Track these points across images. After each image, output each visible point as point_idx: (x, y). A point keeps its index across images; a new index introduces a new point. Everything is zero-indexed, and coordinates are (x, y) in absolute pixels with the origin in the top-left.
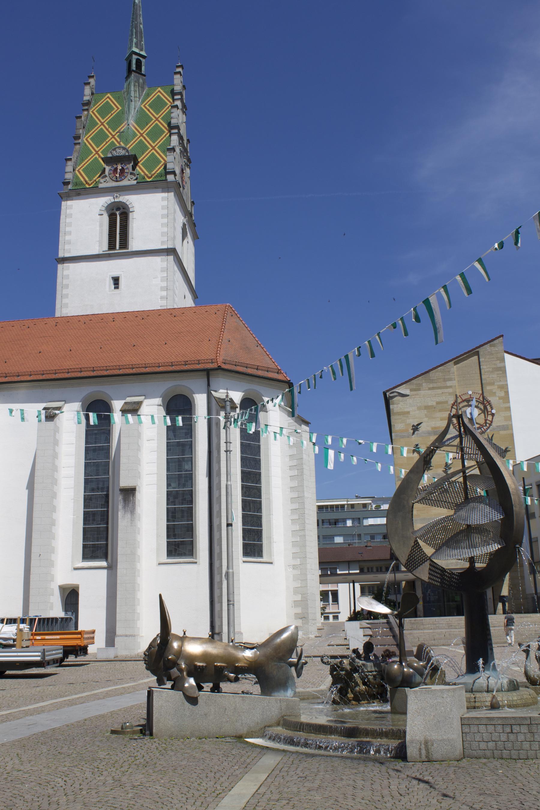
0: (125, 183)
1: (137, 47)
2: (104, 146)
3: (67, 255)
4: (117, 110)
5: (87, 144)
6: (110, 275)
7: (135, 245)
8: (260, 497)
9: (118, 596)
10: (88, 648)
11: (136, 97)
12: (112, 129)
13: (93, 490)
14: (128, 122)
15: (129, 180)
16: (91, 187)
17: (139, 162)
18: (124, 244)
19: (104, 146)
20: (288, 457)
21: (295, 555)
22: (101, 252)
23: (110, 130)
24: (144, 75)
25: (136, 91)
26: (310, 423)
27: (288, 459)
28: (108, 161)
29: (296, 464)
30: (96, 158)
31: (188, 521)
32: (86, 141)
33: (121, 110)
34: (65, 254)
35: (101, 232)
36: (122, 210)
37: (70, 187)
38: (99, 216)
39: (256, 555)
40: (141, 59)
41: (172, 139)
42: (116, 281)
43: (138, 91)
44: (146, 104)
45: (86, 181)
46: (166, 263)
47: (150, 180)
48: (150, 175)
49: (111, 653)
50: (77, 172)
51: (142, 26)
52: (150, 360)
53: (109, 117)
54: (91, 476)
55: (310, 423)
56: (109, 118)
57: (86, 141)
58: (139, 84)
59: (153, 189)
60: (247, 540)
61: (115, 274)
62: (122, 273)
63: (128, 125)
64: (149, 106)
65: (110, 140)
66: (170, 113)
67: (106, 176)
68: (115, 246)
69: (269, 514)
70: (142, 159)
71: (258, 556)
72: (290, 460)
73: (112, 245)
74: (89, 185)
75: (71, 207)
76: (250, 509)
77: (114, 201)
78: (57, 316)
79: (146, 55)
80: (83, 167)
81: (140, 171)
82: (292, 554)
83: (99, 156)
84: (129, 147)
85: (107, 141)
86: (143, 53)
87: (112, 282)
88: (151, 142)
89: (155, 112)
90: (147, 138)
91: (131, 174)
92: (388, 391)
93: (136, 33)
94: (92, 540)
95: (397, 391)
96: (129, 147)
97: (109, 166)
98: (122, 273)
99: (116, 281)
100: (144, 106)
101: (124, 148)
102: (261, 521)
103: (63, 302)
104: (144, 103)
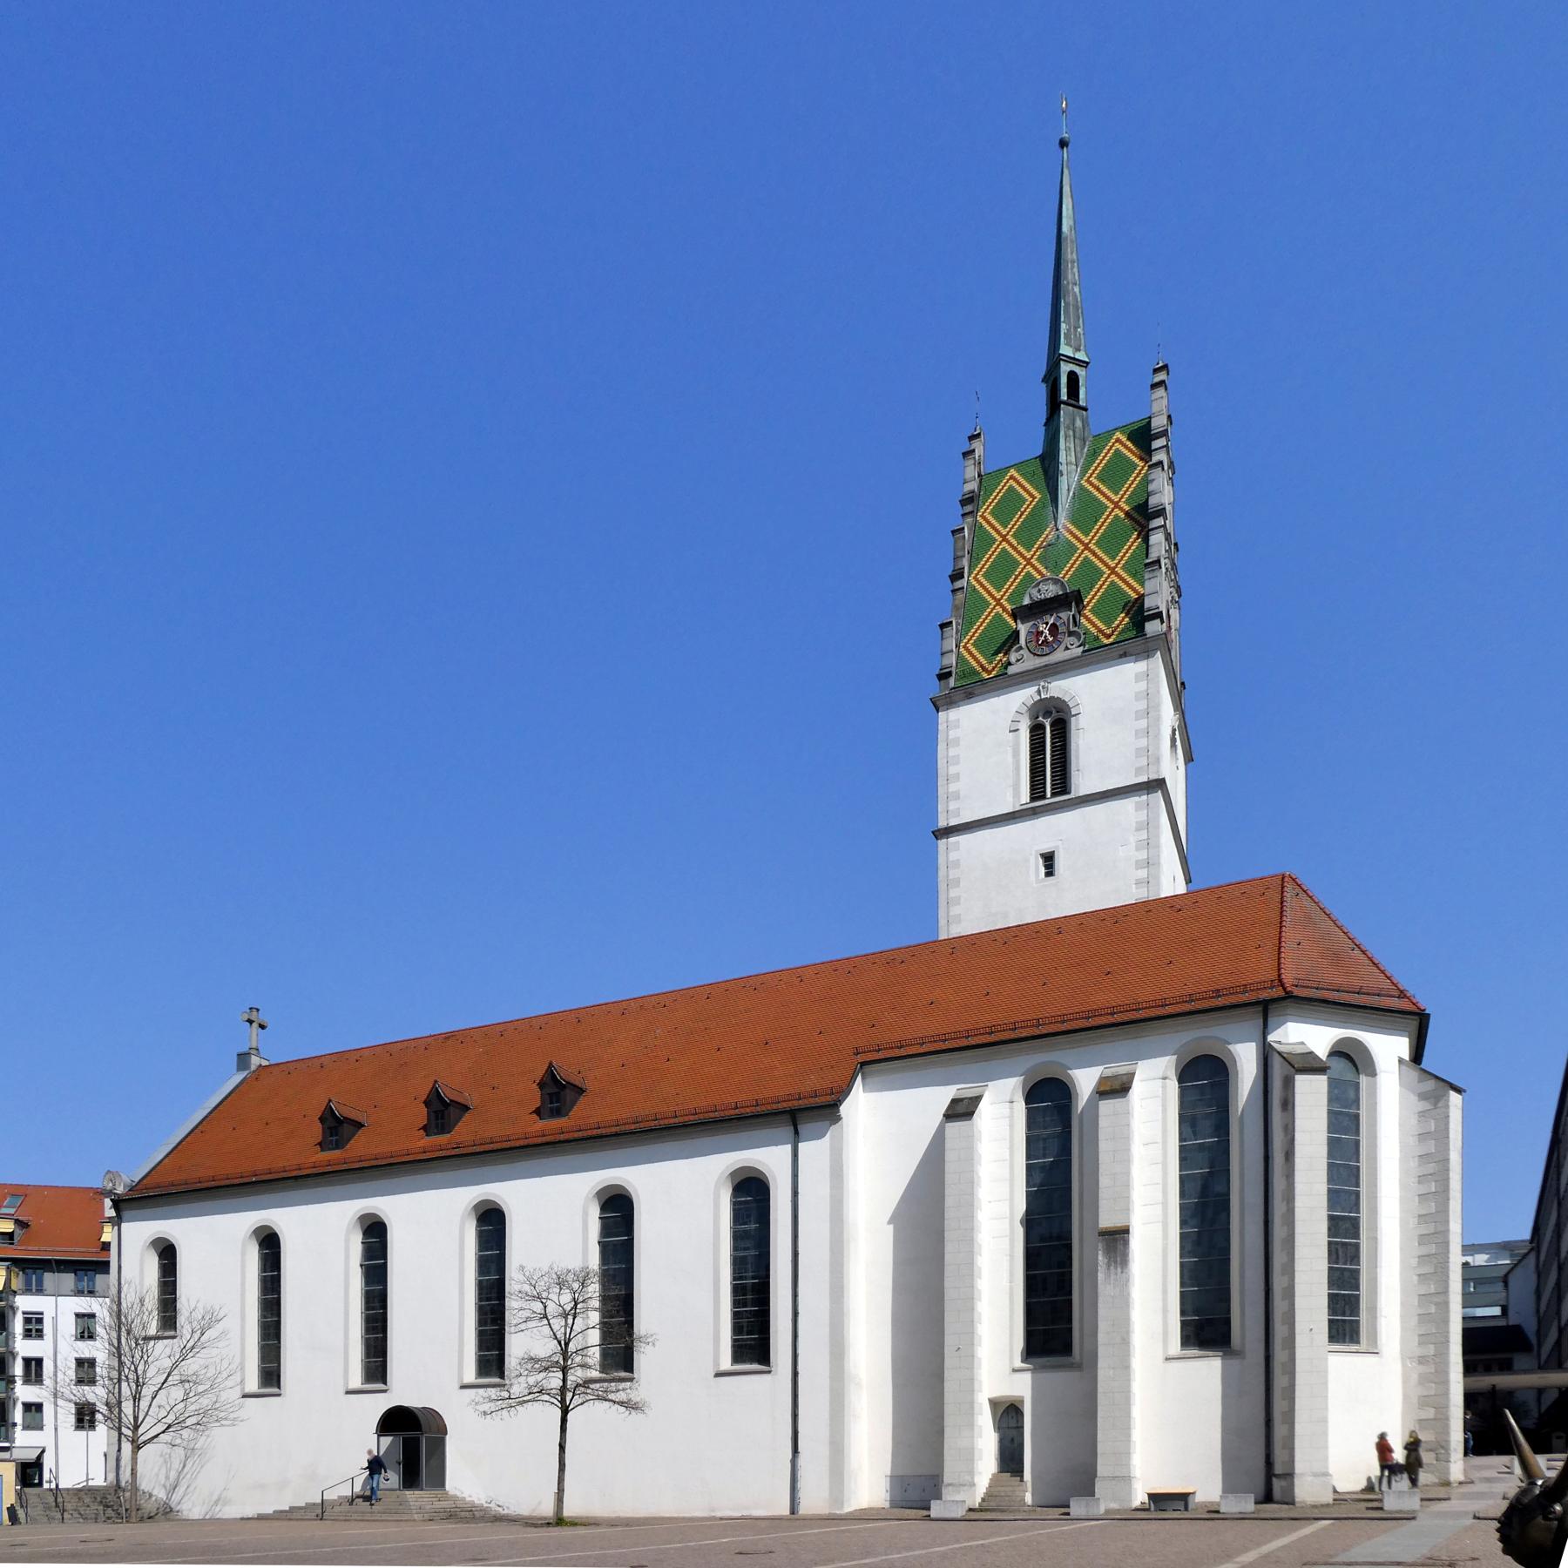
0: (1059, 655)
1: (1068, 344)
2: (1011, 585)
3: (953, 822)
5: (978, 587)
6: (1036, 851)
7: (1084, 781)
9: (1100, 1414)
10: (1220, 1493)
11: (1071, 463)
15: (1067, 648)
17: (1084, 607)
18: (1062, 785)
19: (1011, 585)
20: (1416, 1159)
21: (1424, 1339)
22: (1018, 808)
23: (1020, 548)
24: (1085, 409)
25: (1070, 449)
27: (1417, 1164)
28: (1020, 614)
29: (1432, 1172)
30: (997, 613)
32: (974, 583)
33: (1040, 499)
34: (950, 820)
36: (1055, 714)
37: (952, 682)
39: (1347, 1340)
41: (1151, 543)
42: (1049, 859)
43: (1073, 449)
47: (1111, 640)
48: (1108, 632)
50: (962, 650)
51: (1077, 289)
52: (1146, 994)
53: (1017, 521)
56: (1013, 526)
57: (974, 583)
58: (1074, 431)
60: (1348, 1312)
61: (1046, 848)
63: (1057, 530)
65: (1023, 570)
66: (1146, 481)
67: (1021, 648)
68: (1045, 792)
69: (1374, 1265)
72: (1420, 1165)
73: (1037, 791)
74: (989, 672)
75: (957, 725)
76: (1338, 1258)
77: (1039, 698)
78: (943, 938)
79: (1087, 360)
81: (1089, 626)
83: (1004, 609)
84: (1063, 578)
85: (1017, 573)
86: (1081, 356)
87: (1041, 861)
88: (1106, 558)
89: (1110, 488)
90: (1097, 551)
91: (1071, 634)
96: (1063, 578)
99: (1049, 859)
100: (1088, 481)
101: (1056, 581)
103: (951, 914)
104: (1088, 475)
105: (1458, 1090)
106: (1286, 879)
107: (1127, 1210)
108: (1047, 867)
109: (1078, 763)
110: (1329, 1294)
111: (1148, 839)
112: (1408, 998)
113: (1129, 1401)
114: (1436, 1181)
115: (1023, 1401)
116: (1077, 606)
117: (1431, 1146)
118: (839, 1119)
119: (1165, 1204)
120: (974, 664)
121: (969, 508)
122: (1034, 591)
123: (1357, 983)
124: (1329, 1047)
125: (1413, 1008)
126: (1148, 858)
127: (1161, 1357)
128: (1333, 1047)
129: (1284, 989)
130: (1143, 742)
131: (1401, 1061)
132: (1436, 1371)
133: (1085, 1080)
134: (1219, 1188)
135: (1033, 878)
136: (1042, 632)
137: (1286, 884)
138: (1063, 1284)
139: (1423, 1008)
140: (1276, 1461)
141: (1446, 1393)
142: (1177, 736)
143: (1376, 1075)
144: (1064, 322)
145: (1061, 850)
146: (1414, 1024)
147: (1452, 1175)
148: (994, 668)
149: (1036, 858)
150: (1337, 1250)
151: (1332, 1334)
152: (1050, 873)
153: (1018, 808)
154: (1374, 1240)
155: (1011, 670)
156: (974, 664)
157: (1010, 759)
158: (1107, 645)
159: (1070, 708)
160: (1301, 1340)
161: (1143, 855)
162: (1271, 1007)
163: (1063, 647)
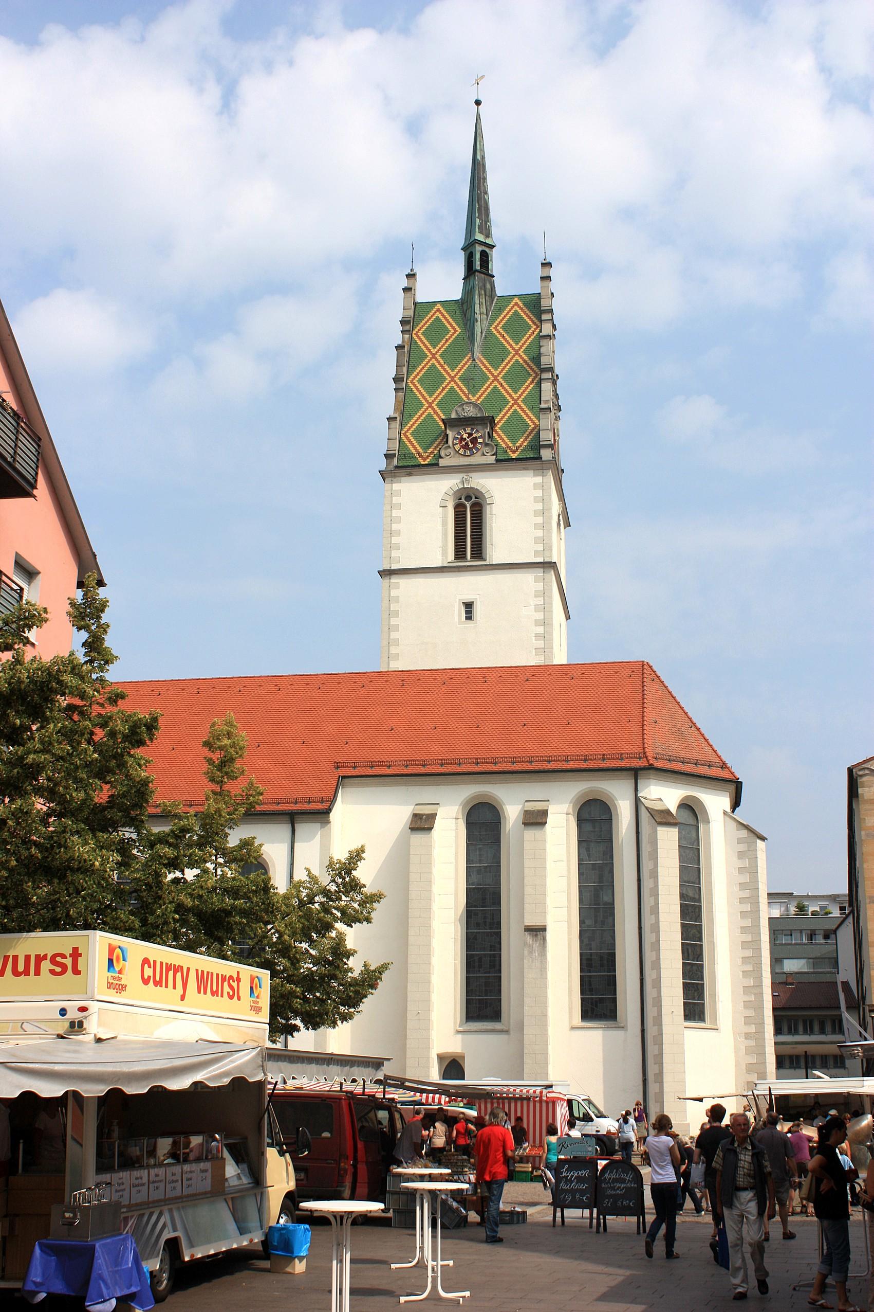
0: (477, 459)
1: (481, 232)
2: (440, 394)
4: (453, 334)
8: (700, 939)
11: (483, 314)
12: (449, 365)
13: (478, 925)
14: (473, 355)
15: (484, 455)
16: (426, 463)
18: (478, 552)
20: (738, 886)
21: (748, 1020)
26: (767, 839)
30: (429, 414)
31: (609, 971)
35: (445, 534)
37: (395, 461)
38: (441, 508)
39: (697, 1019)
40: (487, 250)
42: (469, 607)
43: (484, 304)
44: (498, 325)
45: (419, 454)
46: (542, 584)
49: (177, 1137)
53: (443, 345)
54: (475, 906)
55: (767, 839)
59: (521, 470)
61: (468, 599)
62: (477, 597)
63: (474, 360)
64: (503, 328)
65: (448, 385)
70: (501, 419)
71: (699, 1020)
73: (460, 554)
74: (425, 459)
80: (412, 429)
82: (743, 1019)
89: (512, 338)
92: (854, 766)
93: (479, 209)
94: (478, 994)
95: (869, 767)
97: (452, 432)
98: (477, 597)
99: (469, 607)
102: (702, 972)
105: (763, 839)
106: (645, 667)
107: (544, 913)
108: (467, 612)
109: (491, 540)
110: (683, 982)
111: (544, 604)
112: (728, 768)
113: (547, 1061)
114: (751, 903)
115: (464, 1057)
116: (491, 425)
117: (745, 878)
118: (328, 822)
119: (569, 908)
120: (413, 451)
121: (407, 328)
122: (459, 409)
123: (696, 755)
124: (679, 801)
125: (731, 777)
126: (544, 619)
127: (568, 1027)
128: (682, 800)
129: (648, 761)
130: (540, 533)
131: (725, 813)
132: (756, 1045)
133: (512, 812)
134: (606, 899)
135: (457, 619)
136: (465, 439)
137: (645, 671)
138: (495, 964)
139: (737, 777)
140: (650, 1112)
141: (764, 1063)
142: (561, 518)
143: (709, 822)
144: (478, 218)
145: (479, 603)
146: (732, 787)
147: (761, 900)
148: (428, 457)
149: (459, 603)
150: (688, 949)
151: (686, 1014)
152: (469, 617)
153: (445, 565)
154: (712, 943)
155: (442, 462)
156: (413, 451)
157: (440, 527)
158: (512, 460)
159: (486, 499)
160: (666, 1020)
161: (540, 616)
162: (639, 772)
163: (480, 453)
